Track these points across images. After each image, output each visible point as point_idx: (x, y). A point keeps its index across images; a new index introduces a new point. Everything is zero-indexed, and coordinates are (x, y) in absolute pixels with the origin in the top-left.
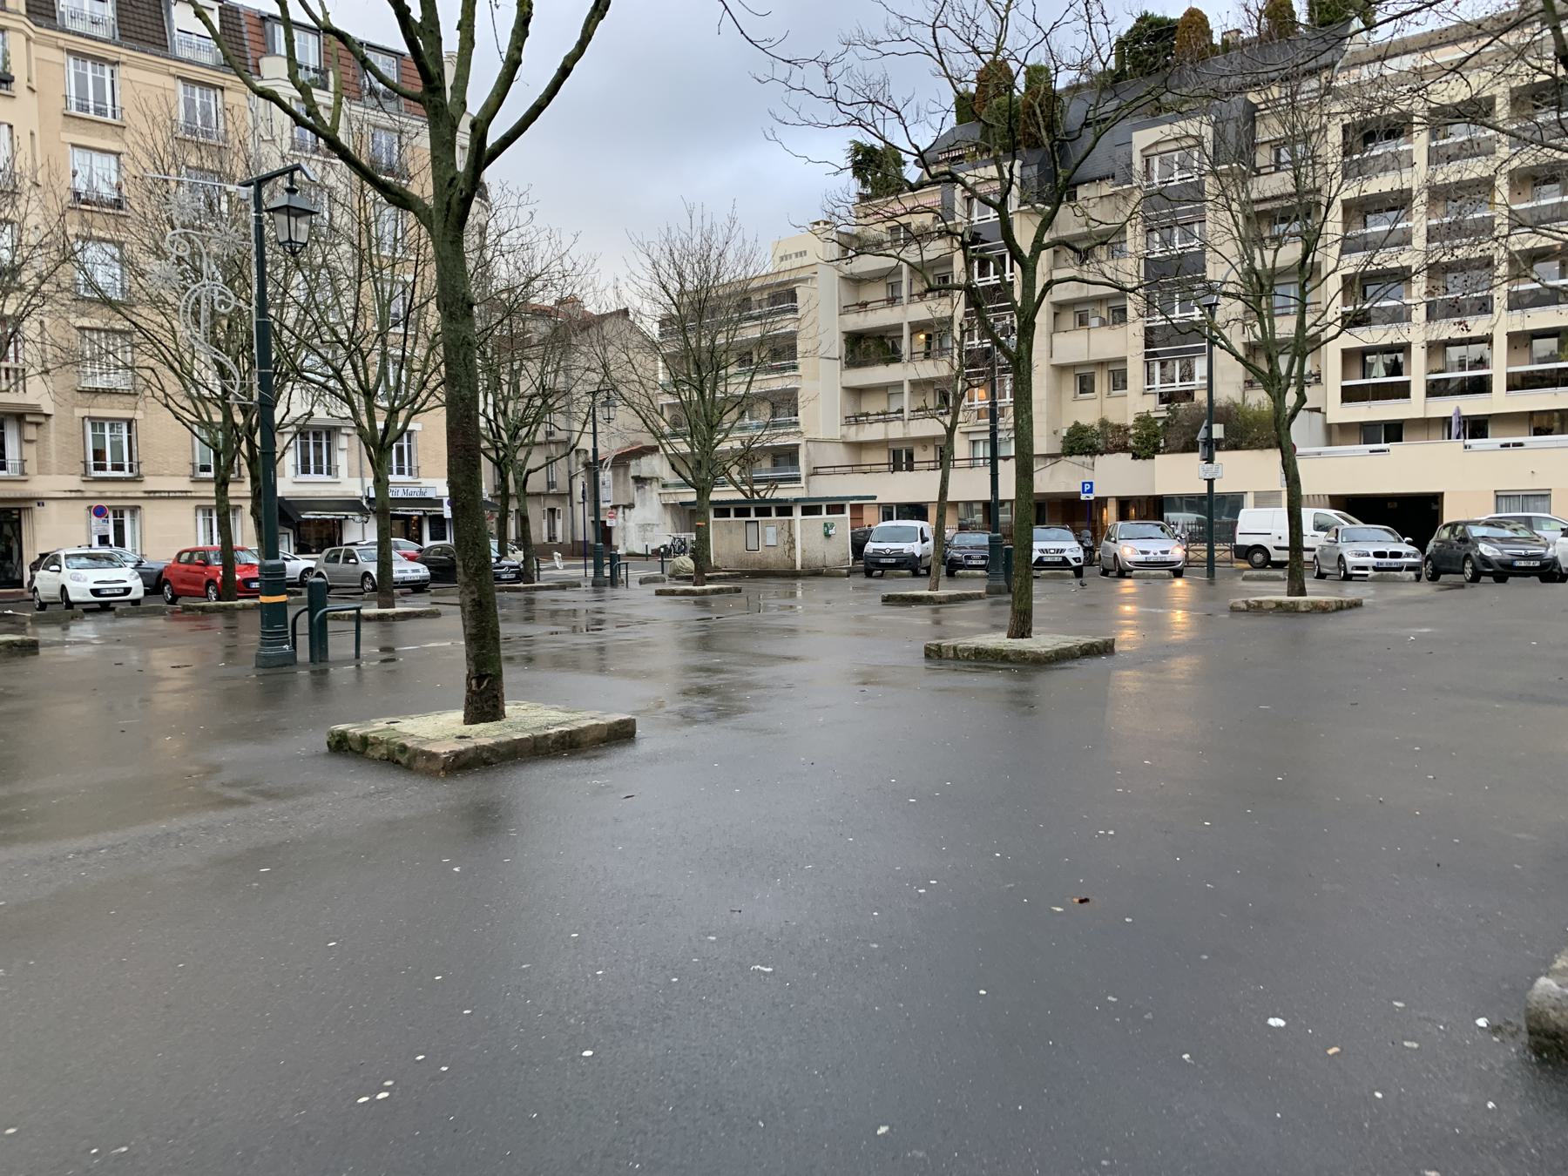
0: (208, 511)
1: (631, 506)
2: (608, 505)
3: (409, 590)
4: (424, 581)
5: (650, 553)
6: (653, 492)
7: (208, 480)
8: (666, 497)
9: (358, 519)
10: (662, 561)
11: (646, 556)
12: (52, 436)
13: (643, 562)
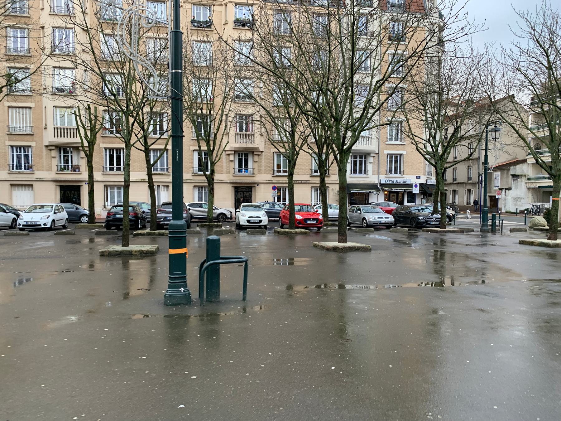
0: (200, 188)
1: (510, 189)
2: (497, 188)
3: (385, 227)
4: (391, 223)
5: (518, 212)
6: (522, 184)
7: (316, 176)
8: (530, 184)
9: (375, 193)
10: (525, 217)
11: (516, 213)
12: (263, 159)
13: (514, 217)
